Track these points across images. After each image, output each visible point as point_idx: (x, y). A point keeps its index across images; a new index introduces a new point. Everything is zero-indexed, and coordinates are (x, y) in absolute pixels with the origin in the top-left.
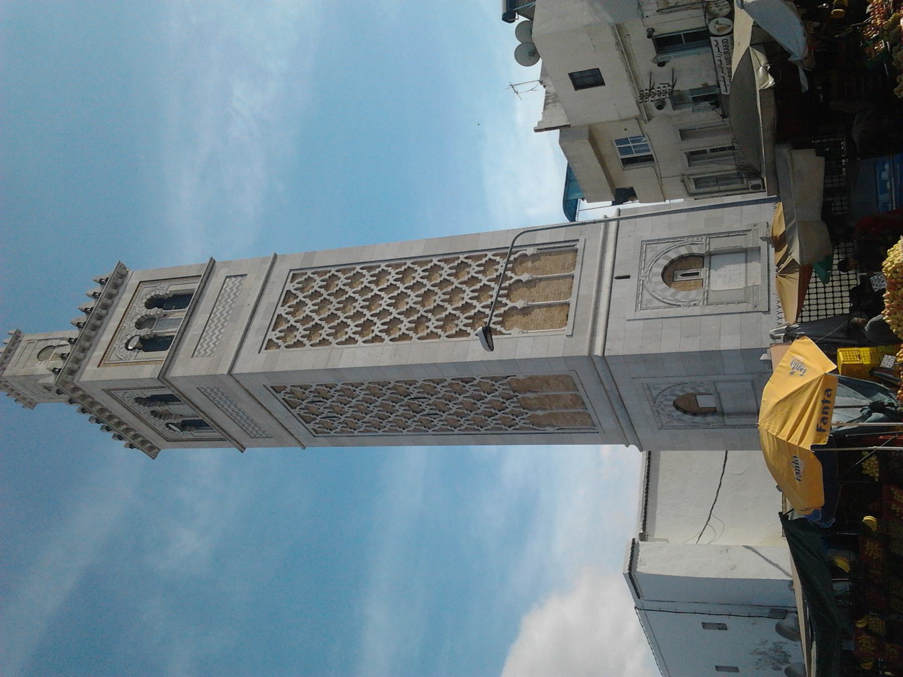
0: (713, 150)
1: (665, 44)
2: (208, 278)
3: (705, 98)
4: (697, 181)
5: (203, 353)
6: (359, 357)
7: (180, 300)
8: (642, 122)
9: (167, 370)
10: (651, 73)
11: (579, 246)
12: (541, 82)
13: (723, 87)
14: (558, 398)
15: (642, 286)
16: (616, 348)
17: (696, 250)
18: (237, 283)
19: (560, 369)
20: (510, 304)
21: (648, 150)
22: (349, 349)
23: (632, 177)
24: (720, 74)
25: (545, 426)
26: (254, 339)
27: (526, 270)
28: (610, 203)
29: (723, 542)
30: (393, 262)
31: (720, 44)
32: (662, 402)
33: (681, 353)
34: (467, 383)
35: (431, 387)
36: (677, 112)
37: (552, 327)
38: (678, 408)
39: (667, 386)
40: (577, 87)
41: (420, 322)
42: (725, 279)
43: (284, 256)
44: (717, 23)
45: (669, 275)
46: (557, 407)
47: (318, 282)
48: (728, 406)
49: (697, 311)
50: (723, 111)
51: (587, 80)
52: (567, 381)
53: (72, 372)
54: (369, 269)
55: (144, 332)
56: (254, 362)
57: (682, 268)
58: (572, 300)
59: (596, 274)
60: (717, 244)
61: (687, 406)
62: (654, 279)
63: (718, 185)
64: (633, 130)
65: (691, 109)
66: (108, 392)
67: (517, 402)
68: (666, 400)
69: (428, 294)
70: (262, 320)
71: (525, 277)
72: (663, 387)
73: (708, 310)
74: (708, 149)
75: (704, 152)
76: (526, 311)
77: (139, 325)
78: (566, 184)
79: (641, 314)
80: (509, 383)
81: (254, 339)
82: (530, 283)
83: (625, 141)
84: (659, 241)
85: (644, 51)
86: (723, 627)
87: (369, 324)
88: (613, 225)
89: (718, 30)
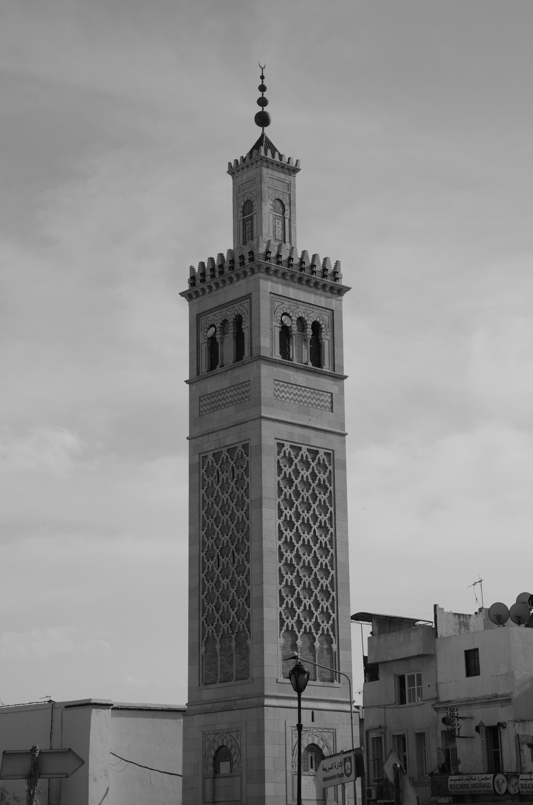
0: (405, 757)
1: (493, 733)
2: (332, 376)
3: (448, 760)
4: (380, 739)
5: (277, 389)
7: (317, 357)
8: (433, 702)
9: (266, 360)
10: (472, 718)
11: (336, 683)
12: (481, 610)
13: (454, 777)
14: (231, 663)
16: (268, 714)
18: (327, 404)
20: (299, 635)
21: (410, 702)
22: (275, 513)
23: (387, 682)
24: (465, 777)
25: (205, 646)
26: (284, 431)
27: (322, 644)
28: (366, 655)
30: (334, 537)
31: (488, 781)
32: (226, 738)
33: (264, 757)
34: (246, 600)
36: (439, 734)
37: (283, 667)
38: (220, 748)
39: (239, 743)
40: (467, 653)
43: (344, 442)
44: (503, 782)
46: (222, 660)
48: (221, 782)
50: (436, 774)
51: (472, 662)
52: (244, 675)
53: (267, 270)
55: (295, 329)
56: (269, 435)
59: (316, 697)
61: (222, 754)
62: (310, 738)
63: (374, 760)
64: (428, 693)
65: (441, 747)
66: (249, 296)
67: (228, 632)
68: (228, 741)
71: (317, 644)
72: (238, 741)
74: (406, 753)
75: (404, 750)
76: (294, 647)
78: (387, 617)
80: (244, 631)
81: (284, 431)
82: (312, 648)
83: (420, 683)
85: (489, 716)
88: (347, 707)
89: (498, 782)
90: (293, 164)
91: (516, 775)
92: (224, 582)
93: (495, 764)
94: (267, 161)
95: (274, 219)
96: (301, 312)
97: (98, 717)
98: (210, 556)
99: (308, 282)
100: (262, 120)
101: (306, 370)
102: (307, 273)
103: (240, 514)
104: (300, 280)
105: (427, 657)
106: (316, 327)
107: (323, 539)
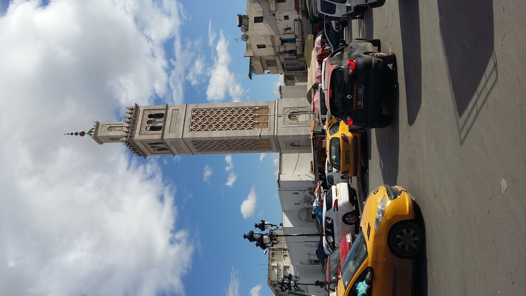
1: (283, 41)
6: (217, 134)
7: (160, 116)
11: (269, 107)
15: (284, 119)
16: (279, 134)
26: (187, 129)
29: (298, 174)
40: (258, 48)
41: (232, 125)
42: (302, 118)
45: (290, 117)
47: (201, 113)
48: (301, 144)
49: (296, 126)
53: (131, 137)
54: (215, 110)
55: (151, 125)
56: (188, 135)
57: (292, 116)
58: (269, 121)
60: (300, 110)
61: (293, 145)
70: (187, 123)
71: (257, 115)
73: (298, 125)
76: (258, 123)
77: (148, 123)
79: (284, 126)
82: (258, 116)
85: (278, 42)
86: (298, 193)
91: (296, 36)
93: (293, 41)
94: (95, 134)
96: (145, 123)
97: (283, 178)
99: (134, 120)
100: (82, 134)
101: (165, 121)
102: (131, 120)
103: (216, 142)
104: (134, 123)
105: (261, 59)
106: (150, 116)
107: (222, 112)
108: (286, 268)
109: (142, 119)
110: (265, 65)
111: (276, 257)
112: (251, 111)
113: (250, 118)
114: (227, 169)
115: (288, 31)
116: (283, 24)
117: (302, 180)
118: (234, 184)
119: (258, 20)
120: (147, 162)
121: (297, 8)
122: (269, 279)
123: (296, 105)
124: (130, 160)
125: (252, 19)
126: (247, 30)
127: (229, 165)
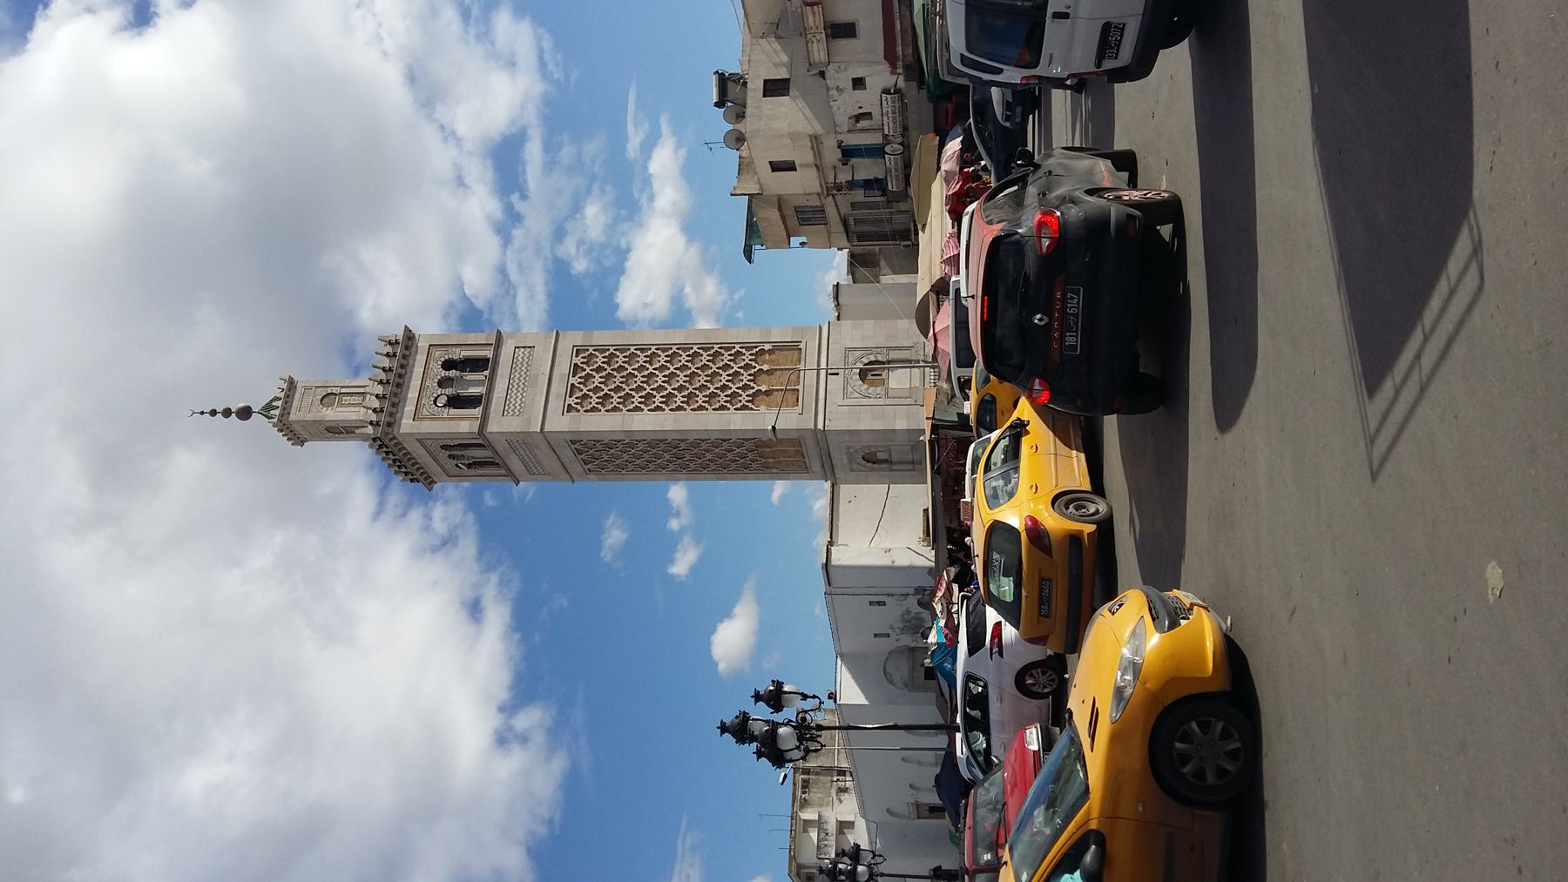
1: (848, 153)
7: (478, 364)
11: (802, 346)
15: (846, 382)
16: (831, 426)
17: (880, 358)
19: (794, 435)
26: (556, 405)
35: (696, 444)
40: (774, 170)
41: (690, 396)
42: (898, 380)
45: (863, 375)
47: (600, 360)
48: (895, 457)
49: (881, 402)
53: (389, 425)
54: (642, 350)
55: (449, 391)
56: (560, 423)
57: (871, 372)
58: (800, 387)
60: (894, 355)
66: (420, 441)
69: (693, 375)
70: (559, 388)
73: (888, 402)
76: (768, 393)
77: (441, 384)
79: (847, 401)
84: (856, 349)
85: (832, 155)
86: (883, 604)
87: (649, 397)
90: (285, 386)
91: (885, 136)
92: (709, 456)
93: (876, 152)
95: (343, 405)
96: (432, 384)
97: (840, 557)
98: (684, 467)
103: (641, 446)
104: (398, 385)
105: (781, 203)
106: (448, 365)
107: (663, 358)
108: (844, 826)
109: (422, 373)
110: (793, 222)
111: (814, 795)
112: (747, 357)
113: (745, 378)
114: (674, 524)
115: (863, 124)
116: (848, 103)
117: (899, 563)
118: (694, 570)
119: (775, 88)
120: (435, 499)
121: (890, 57)
122: (792, 858)
123: (882, 342)
124: (383, 491)
125: (755, 86)
126: (741, 116)
127: (678, 514)
